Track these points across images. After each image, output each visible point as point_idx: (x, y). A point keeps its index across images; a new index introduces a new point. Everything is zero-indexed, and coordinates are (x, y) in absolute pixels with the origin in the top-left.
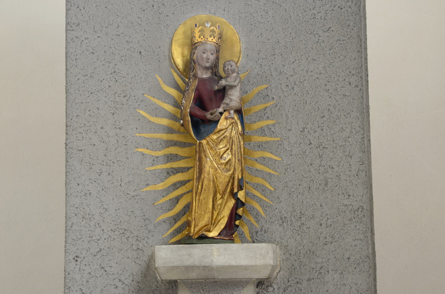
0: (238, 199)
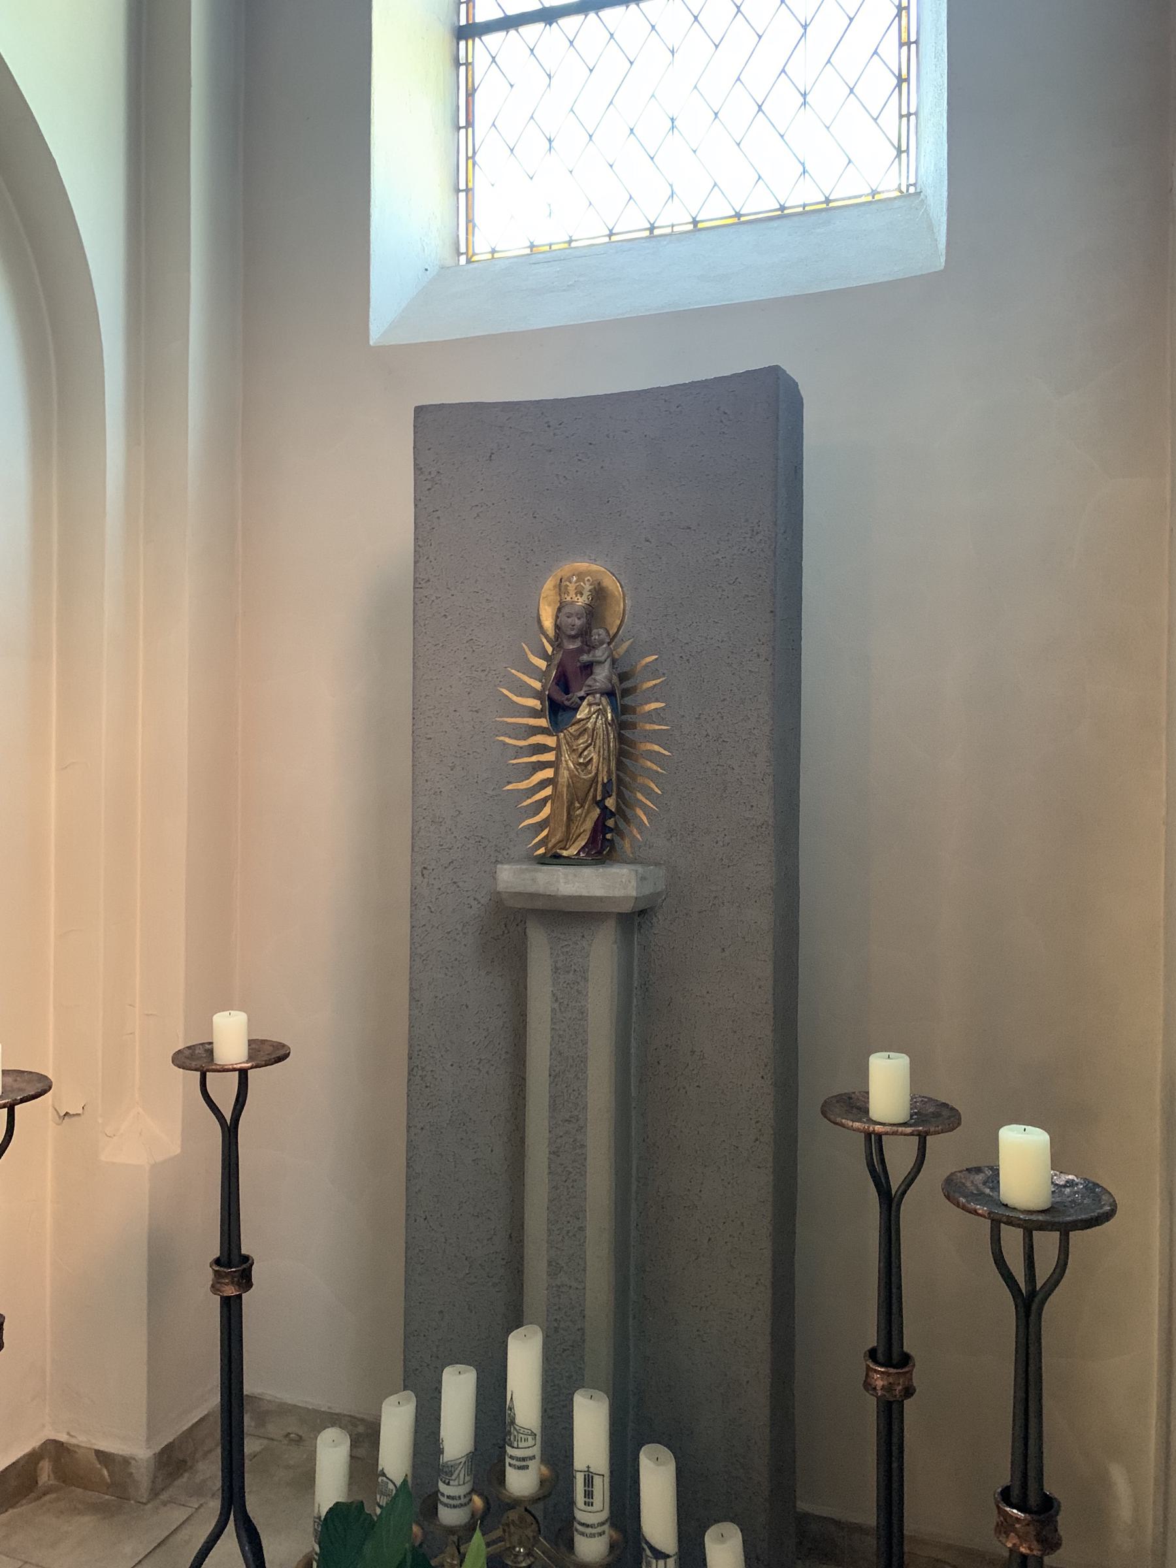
0: (606, 807)
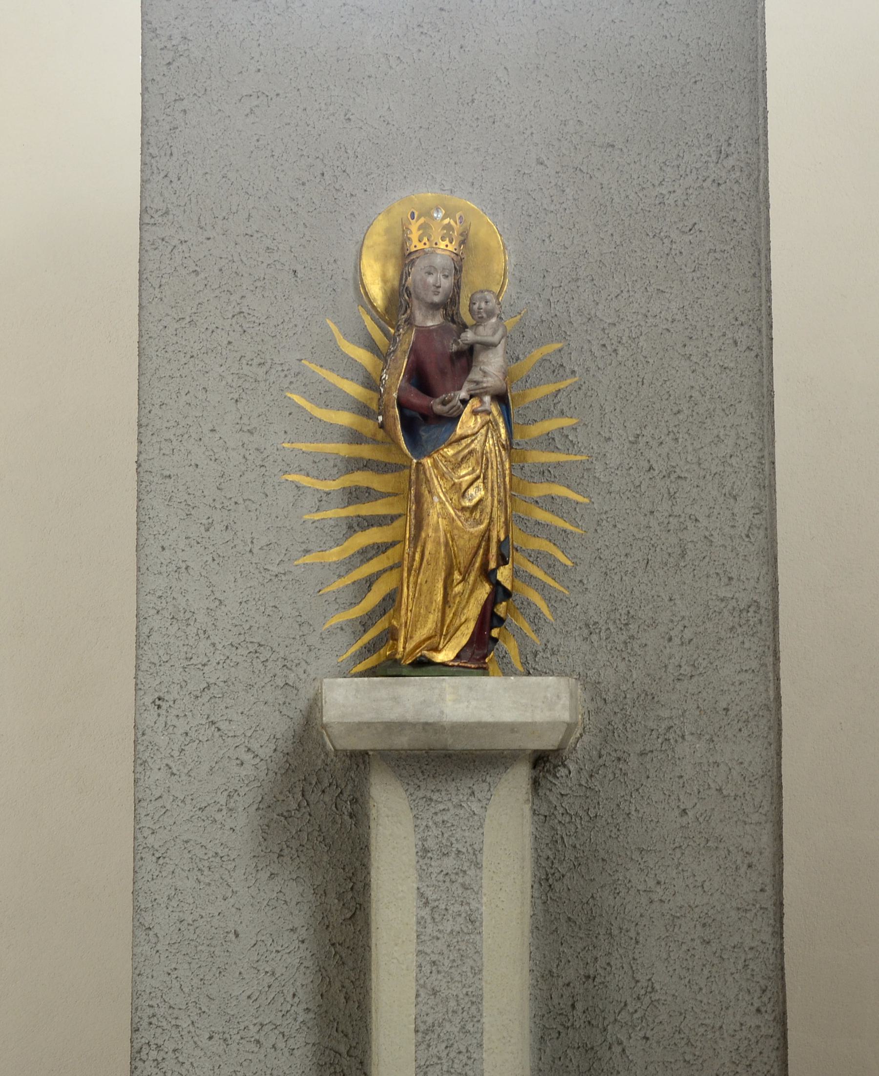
0: (498, 583)
